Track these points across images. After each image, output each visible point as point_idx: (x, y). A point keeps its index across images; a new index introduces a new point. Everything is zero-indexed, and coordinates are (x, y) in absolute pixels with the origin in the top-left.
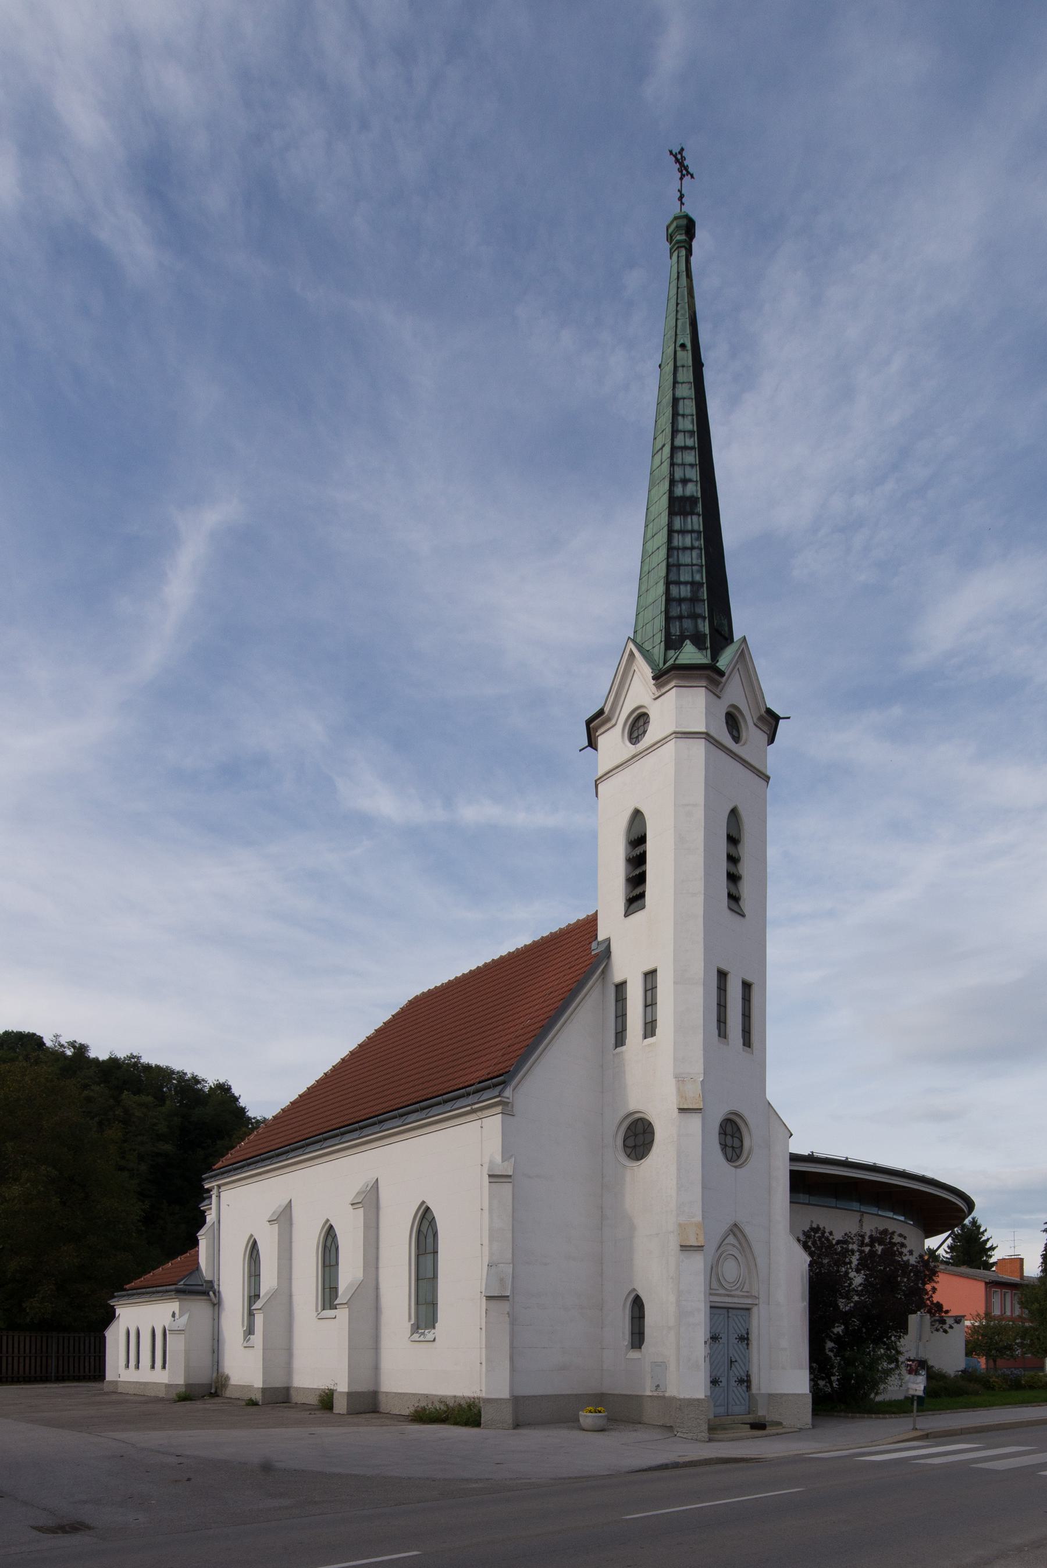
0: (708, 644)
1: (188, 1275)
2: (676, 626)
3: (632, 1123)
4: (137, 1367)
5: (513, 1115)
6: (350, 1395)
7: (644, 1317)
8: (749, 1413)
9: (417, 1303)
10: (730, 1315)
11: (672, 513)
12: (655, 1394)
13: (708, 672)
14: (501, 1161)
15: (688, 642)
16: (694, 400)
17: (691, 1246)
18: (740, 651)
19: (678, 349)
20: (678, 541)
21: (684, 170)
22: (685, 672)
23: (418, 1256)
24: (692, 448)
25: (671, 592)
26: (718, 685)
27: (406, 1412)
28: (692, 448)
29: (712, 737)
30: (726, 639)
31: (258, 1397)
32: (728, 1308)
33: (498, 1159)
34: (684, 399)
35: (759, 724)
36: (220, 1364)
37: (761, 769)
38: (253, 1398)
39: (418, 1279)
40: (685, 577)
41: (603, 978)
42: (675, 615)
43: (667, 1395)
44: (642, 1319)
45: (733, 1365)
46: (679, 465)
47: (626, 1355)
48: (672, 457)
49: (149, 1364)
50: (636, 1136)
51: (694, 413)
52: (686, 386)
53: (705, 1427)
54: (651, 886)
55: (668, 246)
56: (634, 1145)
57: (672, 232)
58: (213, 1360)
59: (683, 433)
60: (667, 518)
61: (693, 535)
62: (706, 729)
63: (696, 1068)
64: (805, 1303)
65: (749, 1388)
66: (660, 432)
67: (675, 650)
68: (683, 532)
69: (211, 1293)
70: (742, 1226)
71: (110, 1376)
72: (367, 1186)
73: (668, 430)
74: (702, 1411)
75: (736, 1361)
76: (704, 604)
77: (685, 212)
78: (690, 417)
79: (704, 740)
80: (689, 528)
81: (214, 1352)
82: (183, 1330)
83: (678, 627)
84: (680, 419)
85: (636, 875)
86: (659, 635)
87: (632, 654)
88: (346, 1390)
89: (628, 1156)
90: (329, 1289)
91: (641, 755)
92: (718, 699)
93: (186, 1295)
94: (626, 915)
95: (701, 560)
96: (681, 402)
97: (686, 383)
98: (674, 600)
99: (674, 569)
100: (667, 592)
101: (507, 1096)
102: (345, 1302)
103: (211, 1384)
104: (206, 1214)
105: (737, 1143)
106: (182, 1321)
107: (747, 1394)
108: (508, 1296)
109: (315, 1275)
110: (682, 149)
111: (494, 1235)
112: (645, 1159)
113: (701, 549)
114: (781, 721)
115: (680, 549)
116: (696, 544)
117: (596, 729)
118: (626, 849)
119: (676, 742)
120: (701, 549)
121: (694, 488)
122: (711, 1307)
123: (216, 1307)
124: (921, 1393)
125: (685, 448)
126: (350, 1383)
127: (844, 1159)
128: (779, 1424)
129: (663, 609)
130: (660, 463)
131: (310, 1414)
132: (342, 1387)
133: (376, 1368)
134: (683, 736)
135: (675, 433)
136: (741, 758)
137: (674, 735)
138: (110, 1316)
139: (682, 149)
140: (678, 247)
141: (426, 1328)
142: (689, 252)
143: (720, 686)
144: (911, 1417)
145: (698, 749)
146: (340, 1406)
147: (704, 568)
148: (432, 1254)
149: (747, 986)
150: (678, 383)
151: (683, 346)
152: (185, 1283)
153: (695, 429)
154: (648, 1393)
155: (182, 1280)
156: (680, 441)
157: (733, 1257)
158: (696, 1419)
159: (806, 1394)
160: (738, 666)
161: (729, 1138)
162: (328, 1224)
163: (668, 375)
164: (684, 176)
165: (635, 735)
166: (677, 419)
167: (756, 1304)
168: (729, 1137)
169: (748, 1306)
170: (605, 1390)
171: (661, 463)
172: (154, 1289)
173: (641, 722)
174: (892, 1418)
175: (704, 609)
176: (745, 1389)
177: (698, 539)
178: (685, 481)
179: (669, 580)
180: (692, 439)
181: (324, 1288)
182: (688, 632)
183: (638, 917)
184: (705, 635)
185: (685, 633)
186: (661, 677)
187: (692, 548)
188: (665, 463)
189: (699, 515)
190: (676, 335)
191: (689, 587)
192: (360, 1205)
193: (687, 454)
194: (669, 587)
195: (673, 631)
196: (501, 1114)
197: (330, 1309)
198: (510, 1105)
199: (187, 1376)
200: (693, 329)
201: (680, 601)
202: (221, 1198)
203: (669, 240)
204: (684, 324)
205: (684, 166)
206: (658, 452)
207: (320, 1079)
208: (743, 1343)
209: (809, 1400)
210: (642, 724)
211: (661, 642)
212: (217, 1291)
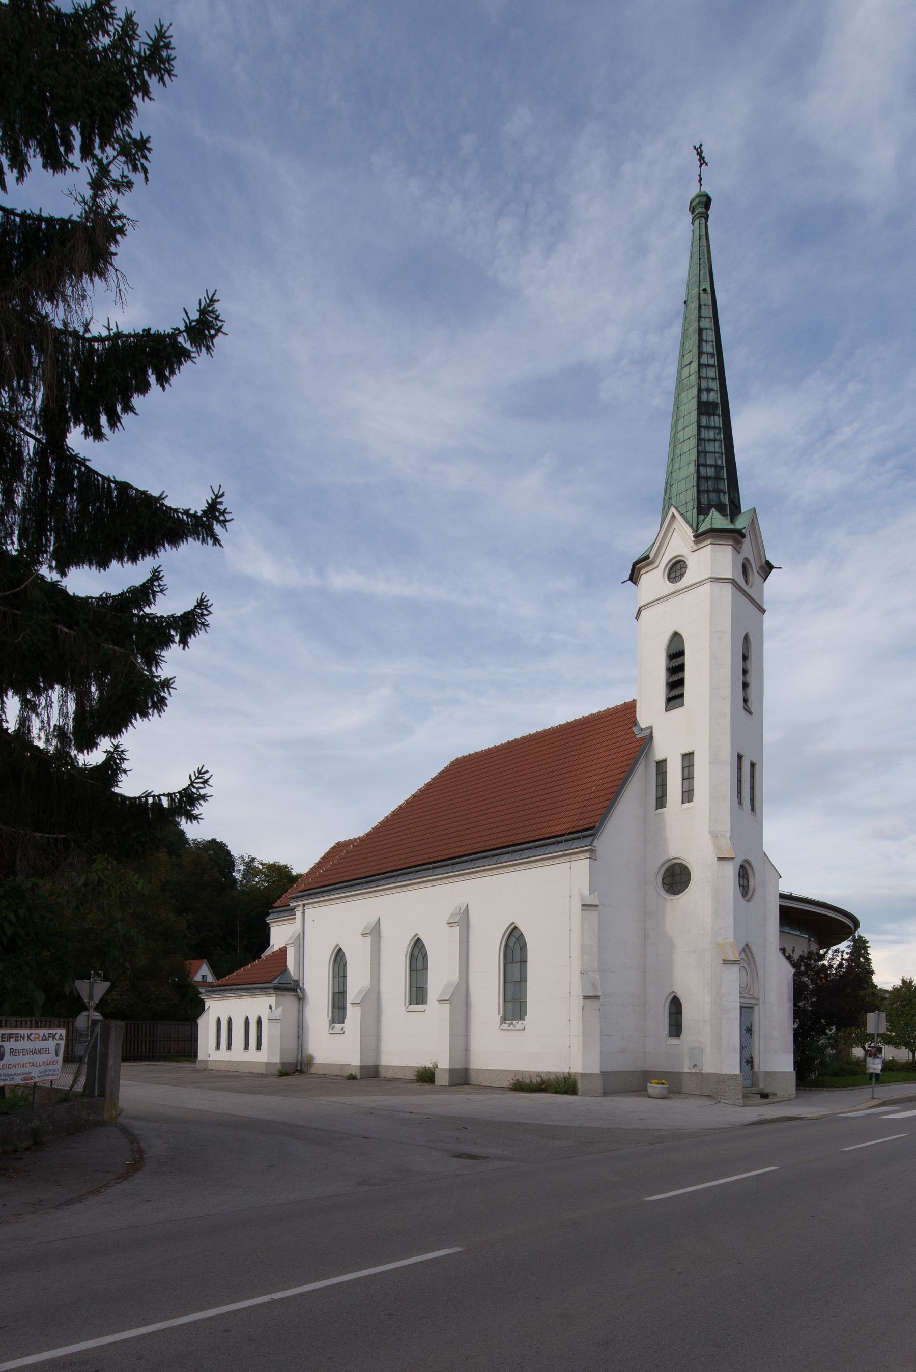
0: (728, 512)
2: (704, 498)
4: (229, 1047)
6: (451, 1071)
7: (681, 1013)
8: (752, 1086)
9: (505, 1001)
11: (700, 414)
12: (693, 1071)
13: (736, 535)
14: (588, 894)
15: (713, 510)
16: (713, 331)
17: (731, 960)
19: (701, 292)
20: (705, 434)
21: (702, 161)
22: (716, 533)
23: (505, 964)
24: (713, 366)
26: (739, 544)
27: (507, 1084)
28: (713, 366)
29: (736, 583)
31: (357, 1073)
33: (586, 892)
34: (706, 329)
35: (760, 572)
36: (303, 1047)
37: (761, 604)
38: (353, 1074)
39: (505, 982)
40: (710, 461)
43: (703, 1072)
46: (704, 378)
48: (699, 371)
49: (242, 1046)
50: (673, 877)
51: (714, 341)
53: (741, 1096)
57: (695, 205)
58: (298, 1045)
60: (696, 417)
62: (733, 576)
63: (725, 826)
64: (791, 1004)
65: (752, 1067)
67: (705, 515)
68: (708, 428)
69: (298, 990)
70: (750, 945)
71: (201, 1056)
73: (695, 351)
74: (739, 1083)
75: (746, 1047)
78: (711, 343)
80: (713, 425)
81: (299, 1037)
82: (280, 1019)
83: (706, 497)
84: (704, 344)
85: (675, 681)
86: (692, 503)
87: (673, 516)
88: (448, 1067)
89: (667, 891)
90: (416, 989)
91: (683, 591)
92: (738, 554)
93: (282, 991)
94: (666, 710)
96: (704, 331)
97: (708, 317)
98: (703, 478)
99: (702, 455)
100: (698, 471)
101: (595, 845)
102: (448, 999)
103: (297, 1063)
106: (278, 1012)
107: (751, 1071)
108: (600, 996)
109: (404, 977)
110: (701, 145)
111: (584, 951)
112: (683, 893)
116: (718, 437)
117: (640, 569)
118: (666, 661)
119: (711, 585)
120: (721, 441)
123: (301, 1001)
125: (708, 366)
126: (451, 1061)
127: (789, 894)
128: (776, 1094)
129: (695, 484)
131: (420, 1085)
132: (444, 1064)
133: (467, 1050)
137: (710, 580)
138: (200, 1008)
139: (701, 145)
140: (699, 217)
141: (513, 1019)
146: (442, 1079)
147: (724, 455)
148: (520, 963)
149: (753, 765)
150: (702, 317)
151: (705, 290)
153: (715, 352)
154: (686, 1070)
155: (275, 978)
156: (704, 360)
158: (735, 1089)
159: (791, 1072)
163: (694, 310)
165: (673, 575)
166: (702, 344)
167: (757, 1004)
168: (741, 878)
169: (750, 1005)
171: (690, 375)
172: (239, 987)
173: (678, 567)
174: (838, 1091)
175: (724, 486)
176: (749, 1067)
177: (719, 433)
178: (709, 390)
180: (713, 360)
181: (410, 988)
183: (677, 713)
186: (699, 537)
187: (715, 440)
188: (693, 376)
190: (699, 281)
191: (713, 469)
192: (457, 924)
194: (699, 469)
195: (702, 501)
199: (281, 1058)
201: (707, 479)
202: (305, 914)
203: (691, 210)
204: (705, 273)
206: (686, 366)
209: (794, 1076)
211: (694, 508)
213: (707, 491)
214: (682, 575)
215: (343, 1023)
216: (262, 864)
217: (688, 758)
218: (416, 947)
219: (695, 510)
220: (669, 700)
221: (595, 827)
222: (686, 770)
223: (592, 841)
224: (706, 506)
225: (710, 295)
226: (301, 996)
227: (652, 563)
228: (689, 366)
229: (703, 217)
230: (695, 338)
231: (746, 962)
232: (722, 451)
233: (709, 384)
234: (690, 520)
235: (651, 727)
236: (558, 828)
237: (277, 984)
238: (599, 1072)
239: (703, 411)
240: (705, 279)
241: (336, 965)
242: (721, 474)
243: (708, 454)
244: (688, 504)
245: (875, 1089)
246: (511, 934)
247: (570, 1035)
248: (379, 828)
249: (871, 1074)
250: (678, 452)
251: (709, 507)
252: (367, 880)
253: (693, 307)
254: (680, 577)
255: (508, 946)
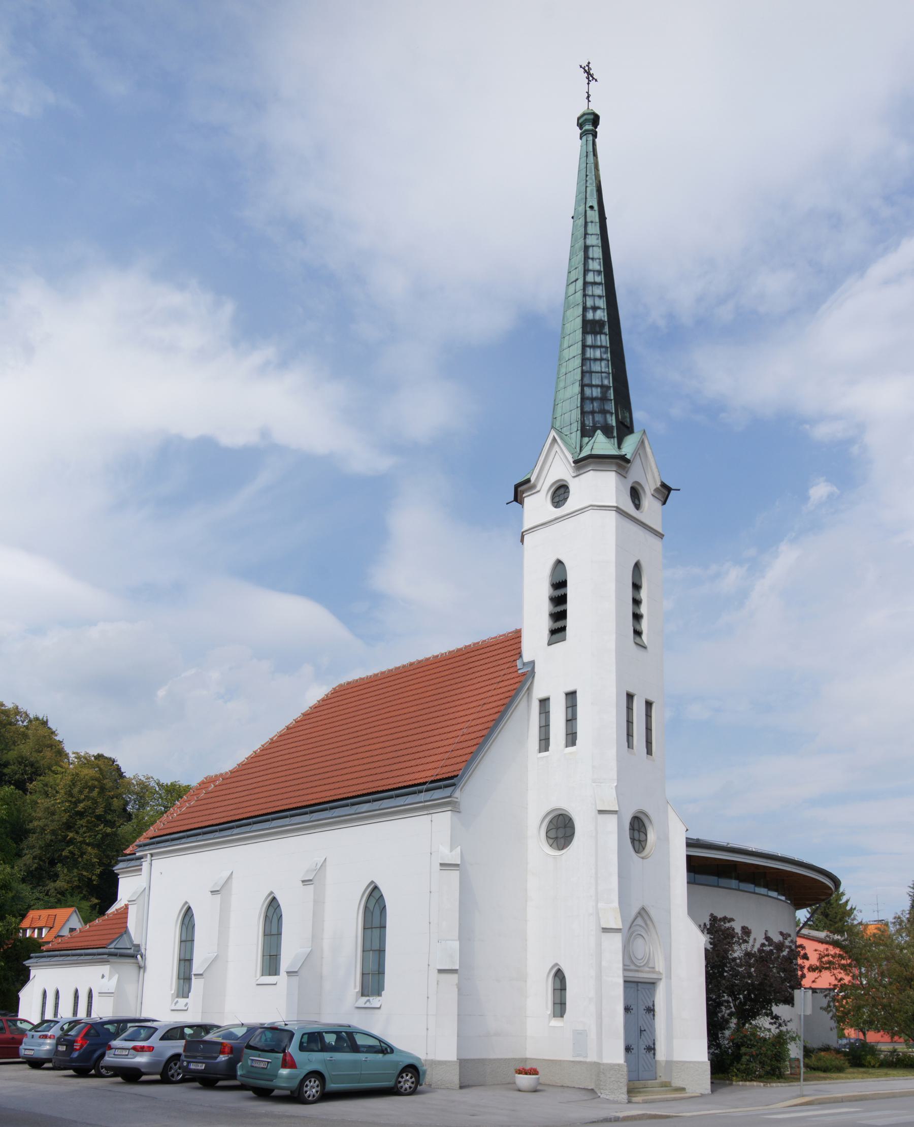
0: (615, 434)
1: (117, 938)
2: (589, 420)
3: (554, 818)
5: (459, 812)
10: (639, 988)
11: (585, 332)
15: (599, 432)
18: (641, 441)
19: (588, 209)
20: (590, 353)
24: (600, 284)
25: (585, 393)
28: (600, 284)
30: (627, 427)
32: (637, 983)
34: (593, 246)
41: (528, 694)
42: (589, 410)
45: (642, 1034)
46: (589, 296)
47: (549, 1024)
48: (584, 289)
52: (594, 237)
53: (625, 1090)
54: (571, 621)
55: (578, 131)
56: (555, 836)
57: (582, 122)
59: (592, 272)
60: (581, 336)
61: (602, 349)
66: (574, 268)
67: (589, 437)
68: (594, 347)
69: (139, 957)
70: (648, 909)
72: (317, 865)
74: (622, 1075)
75: (645, 1030)
76: (612, 403)
77: (592, 110)
78: (598, 261)
79: (614, 512)
80: (599, 344)
83: (591, 420)
84: (590, 261)
86: (575, 424)
94: (550, 644)
95: (609, 369)
96: (591, 249)
97: (594, 234)
98: (588, 398)
100: (582, 392)
101: (457, 797)
104: (119, 877)
105: (642, 837)
113: (608, 360)
114: (672, 491)
115: (592, 360)
116: (604, 356)
120: (608, 360)
121: (602, 314)
122: (625, 982)
123: (142, 971)
125: (594, 283)
127: (726, 844)
129: (579, 405)
130: (574, 292)
134: (598, 508)
135: (586, 272)
136: (642, 522)
138: (23, 977)
139: (589, 63)
142: (595, 135)
143: (626, 469)
144: (798, 1085)
150: (589, 234)
152: (116, 947)
153: (602, 269)
156: (590, 277)
157: (640, 937)
160: (639, 451)
161: (636, 833)
162: (272, 895)
164: (587, 66)
166: (588, 262)
171: (575, 293)
173: (562, 490)
175: (611, 406)
177: (606, 352)
178: (595, 309)
179: (584, 383)
180: (600, 277)
182: (599, 424)
184: (613, 426)
185: (596, 424)
187: (601, 359)
189: (606, 335)
191: (599, 390)
193: (596, 288)
195: (587, 422)
196: (450, 812)
197: (270, 975)
198: (457, 804)
200: (599, 194)
201: (592, 399)
204: (592, 190)
205: (590, 74)
206: (572, 283)
207: (249, 756)
208: (650, 1014)
210: (563, 493)
211: (578, 430)
212: (144, 954)
214: (566, 499)
215: (188, 997)
216: (158, 784)
218: (371, 897)
219: (579, 432)
220: (553, 632)
221: (458, 775)
222: (570, 710)
223: (454, 790)
224: (590, 428)
225: (597, 212)
226: (142, 963)
228: (575, 283)
229: (591, 133)
230: (581, 255)
231: (644, 928)
232: (609, 370)
233: (596, 302)
235: (533, 663)
237: (113, 950)
238: (455, 1059)
239: (588, 330)
241: (184, 927)
242: (608, 395)
243: (593, 374)
244: (572, 425)
246: (370, 895)
247: (427, 1015)
248: (245, 764)
250: (563, 370)
251: (594, 429)
252: (188, 833)
253: (580, 224)
254: (563, 501)
255: (367, 908)
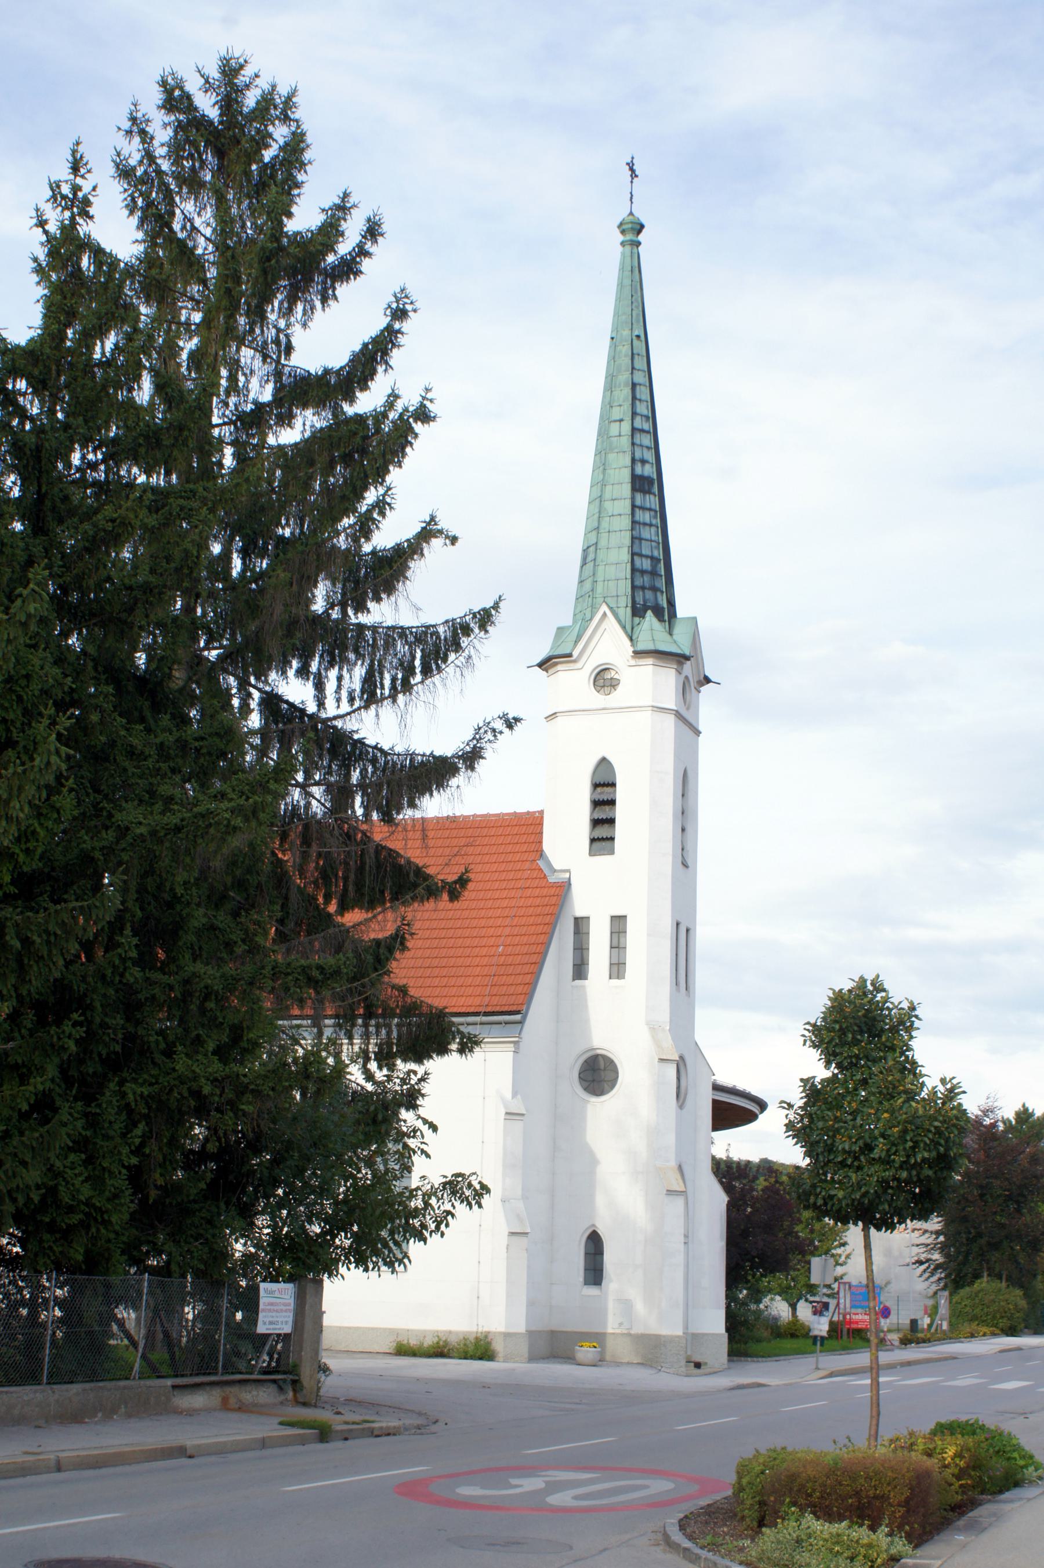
0: (666, 617)
7: (602, 1253)
11: (634, 489)
12: (618, 1331)
21: (633, 174)
33: (508, 1095)
37: (694, 724)
40: (646, 551)
44: (598, 1257)
73: (627, 407)
84: (638, 402)
87: (605, 614)
96: (638, 387)
98: (638, 570)
99: (637, 542)
116: (654, 522)
124: (824, 1334)
125: (642, 431)
129: (629, 576)
145: (670, 720)
151: (638, 337)
170: (554, 1328)
175: (661, 583)
178: (643, 462)
191: (649, 561)
195: (637, 599)
201: (643, 572)
204: (638, 315)
213: (643, 588)
217: (619, 924)
219: (629, 610)
222: (615, 936)
227: (575, 661)
234: (622, 619)
236: (462, 1001)
239: (637, 487)
240: (638, 321)
245: (820, 1359)
249: (815, 1337)
251: (646, 607)
